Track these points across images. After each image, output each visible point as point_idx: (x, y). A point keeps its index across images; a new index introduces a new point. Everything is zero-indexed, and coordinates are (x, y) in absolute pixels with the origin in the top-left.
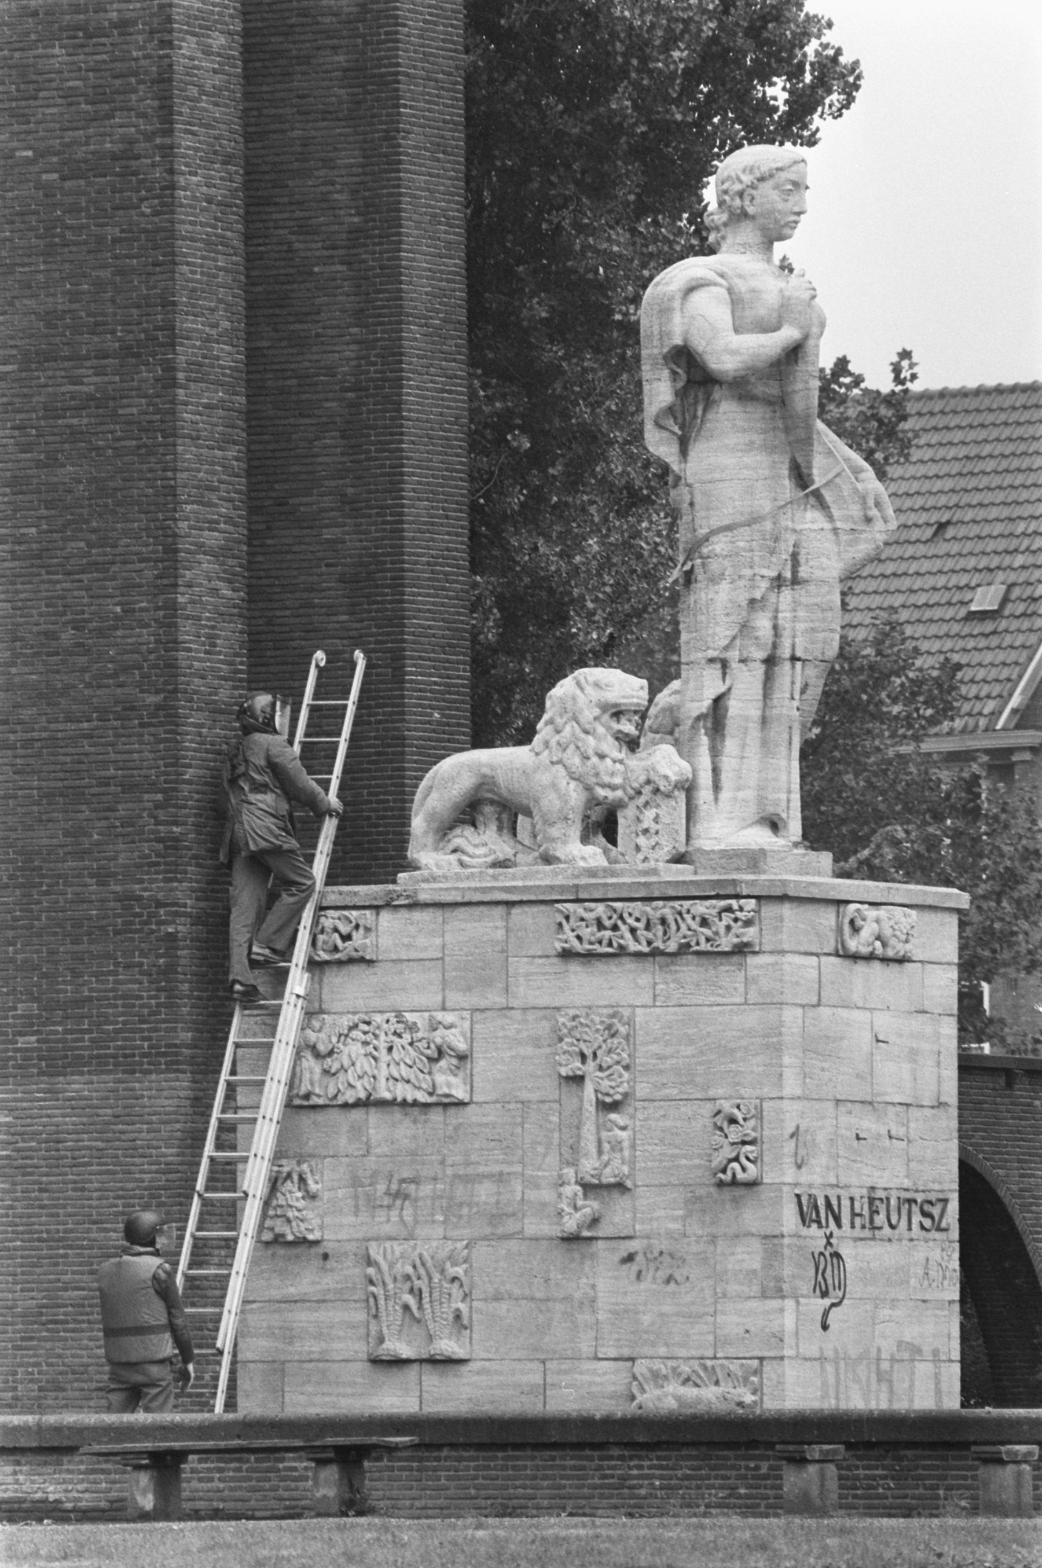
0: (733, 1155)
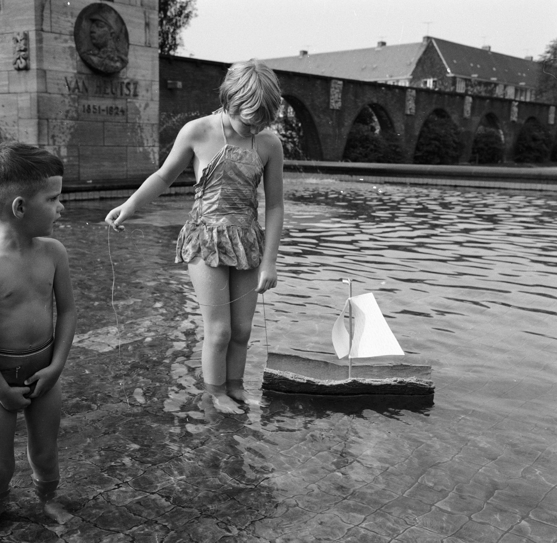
0: (18, 57)
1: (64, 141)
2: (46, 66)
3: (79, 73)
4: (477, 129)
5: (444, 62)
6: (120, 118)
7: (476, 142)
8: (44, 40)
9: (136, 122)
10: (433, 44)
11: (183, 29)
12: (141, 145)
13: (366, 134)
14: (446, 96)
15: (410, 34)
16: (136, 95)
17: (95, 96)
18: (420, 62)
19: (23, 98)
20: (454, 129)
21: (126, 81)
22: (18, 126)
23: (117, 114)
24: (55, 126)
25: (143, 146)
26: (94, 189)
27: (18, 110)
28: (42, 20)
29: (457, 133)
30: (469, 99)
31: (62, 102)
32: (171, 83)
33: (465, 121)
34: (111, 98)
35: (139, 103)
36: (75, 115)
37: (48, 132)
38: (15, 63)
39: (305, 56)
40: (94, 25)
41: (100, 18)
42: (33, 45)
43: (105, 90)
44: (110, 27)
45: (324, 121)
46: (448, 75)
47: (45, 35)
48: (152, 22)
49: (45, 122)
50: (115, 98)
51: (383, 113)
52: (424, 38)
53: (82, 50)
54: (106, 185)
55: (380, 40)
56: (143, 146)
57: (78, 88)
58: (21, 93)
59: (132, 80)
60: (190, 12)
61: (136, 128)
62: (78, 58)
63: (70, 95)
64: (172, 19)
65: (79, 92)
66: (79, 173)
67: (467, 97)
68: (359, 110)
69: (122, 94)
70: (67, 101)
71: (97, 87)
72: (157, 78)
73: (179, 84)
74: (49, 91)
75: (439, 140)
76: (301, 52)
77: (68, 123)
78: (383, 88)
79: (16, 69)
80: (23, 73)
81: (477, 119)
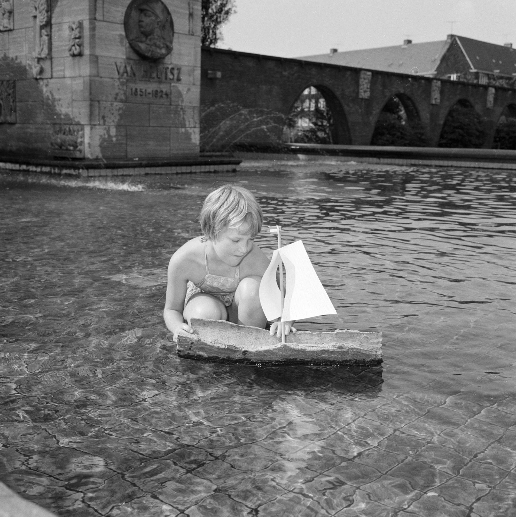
1: (113, 121)
2: (98, 52)
3: (128, 59)
4: (499, 120)
5: (468, 59)
6: (164, 101)
7: (498, 131)
8: (97, 28)
9: (179, 105)
10: (456, 42)
11: (223, 24)
12: (184, 126)
13: (393, 122)
14: (470, 87)
15: (434, 32)
16: (179, 80)
17: (142, 80)
18: (444, 59)
19: (77, 82)
20: (477, 119)
21: (170, 67)
22: (72, 107)
23: (161, 96)
24: (105, 108)
25: (185, 127)
26: (140, 166)
27: (72, 93)
28: (96, 10)
29: (480, 123)
30: (492, 90)
31: (111, 79)
32: (211, 74)
33: (488, 111)
34: (156, 82)
35: (181, 87)
36: (123, 97)
37: (99, 113)
38: (70, 50)
39: (335, 53)
40: (143, 15)
41: (148, 8)
42: (87, 33)
43: (151, 75)
44: (157, 17)
45: (353, 109)
46: (471, 71)
47: (97, 24)
48: (195, 12)
49: (96, 104)
50: (160, 82)
51: (409, 102)
52: (448, 36)
53: (131, 38)
54: (150, 162)
55: (406, 38)
56: (185, 127)
57: (127, 72)
58: (76, 77)
59: (176, 65)
60: (230, 9)
61: (178, 110)
62: (128, 45)
63: (119, 79)
64: (212, 16)
65: (127, 76)
66: (126, 151)
67: (490, 88)
68: (386, 99)
69: (166, 79)
70: (116, 84)
71: (144, 71)
72: (199, 64)
73: (219, 74)
74: (102, 75)
75: (462, 129)
76: (331, 50)
77: (117, 105)
78: (410, 79)
79: (71, 55)
80: (77, 58)
81: (499, 110)
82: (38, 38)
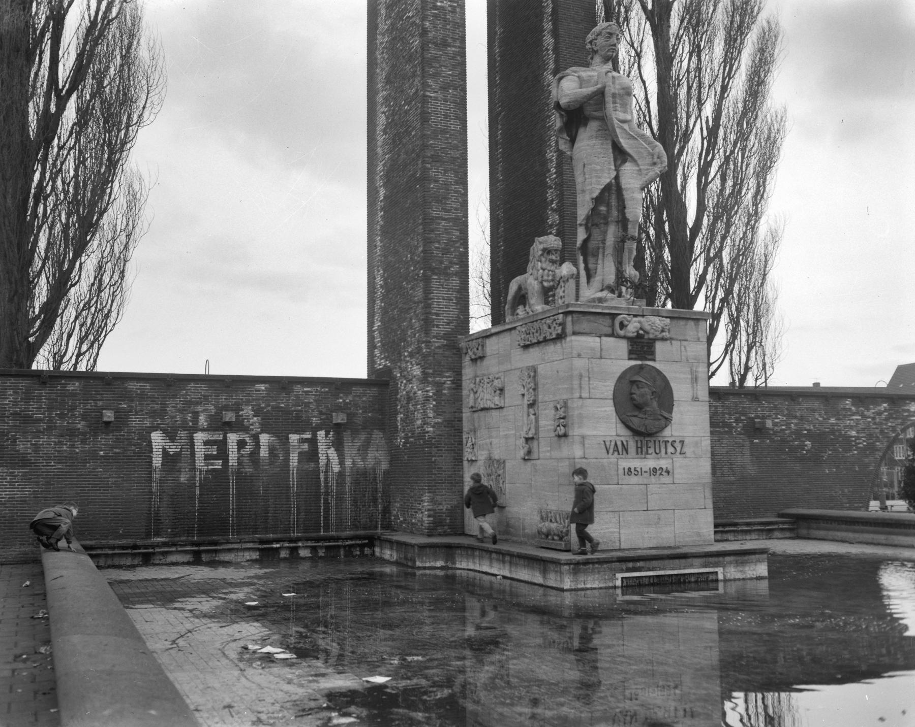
21: (670, 440)
80: (563, 439)
82: (525, 418)
